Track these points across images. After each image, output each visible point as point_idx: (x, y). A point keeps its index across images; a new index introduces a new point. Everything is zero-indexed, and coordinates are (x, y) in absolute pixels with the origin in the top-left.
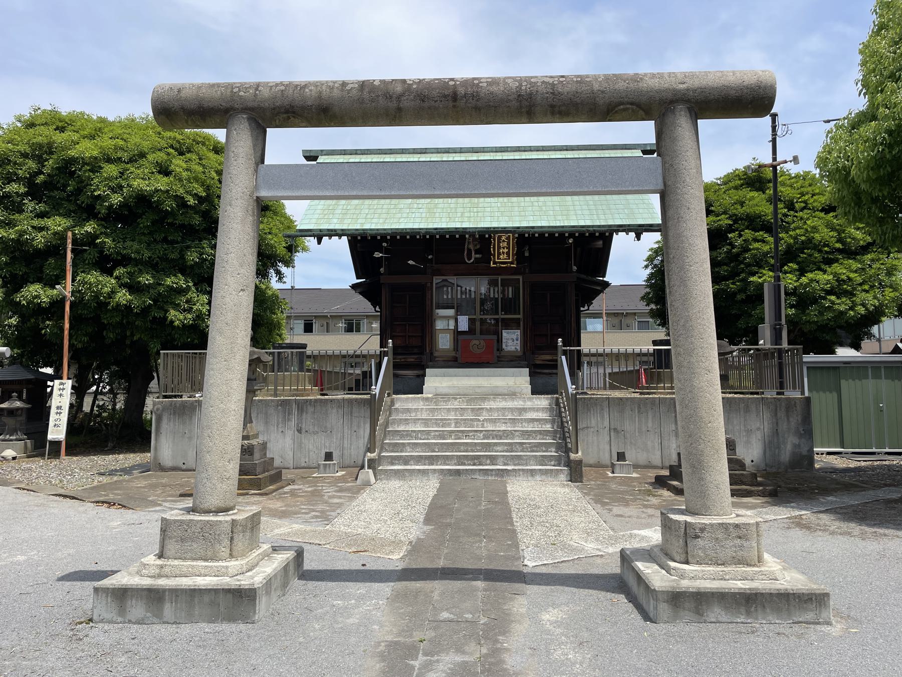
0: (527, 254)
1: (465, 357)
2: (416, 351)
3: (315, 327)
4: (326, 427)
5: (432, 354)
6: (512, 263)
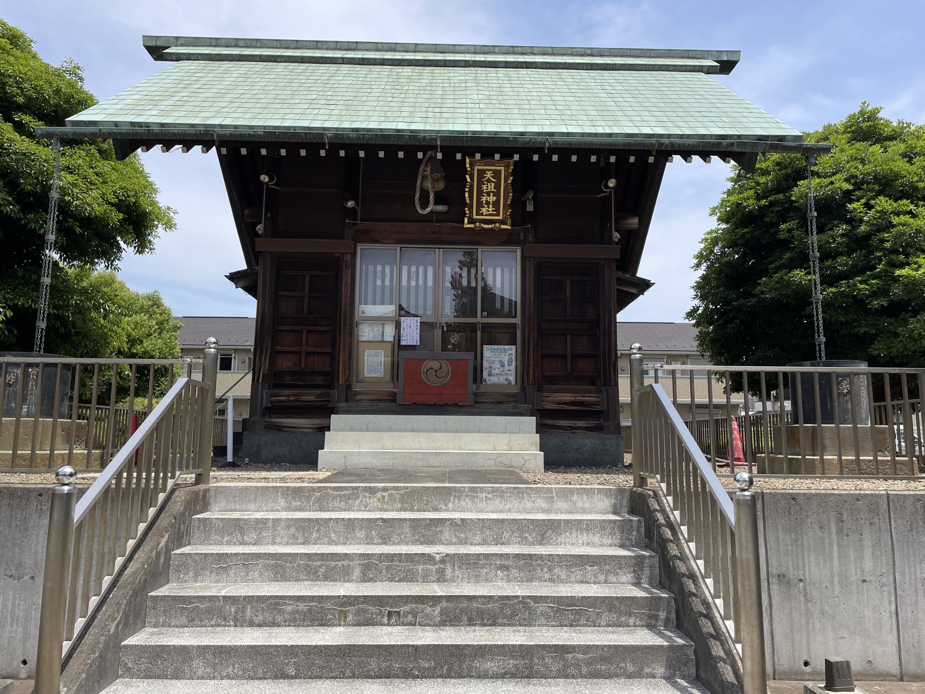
0: (530, 208)
1: (415, 392)
2: (319, 380)
3: (234, 363)
4: (20, 565)
5: (349, 387)
6: (503, 222)
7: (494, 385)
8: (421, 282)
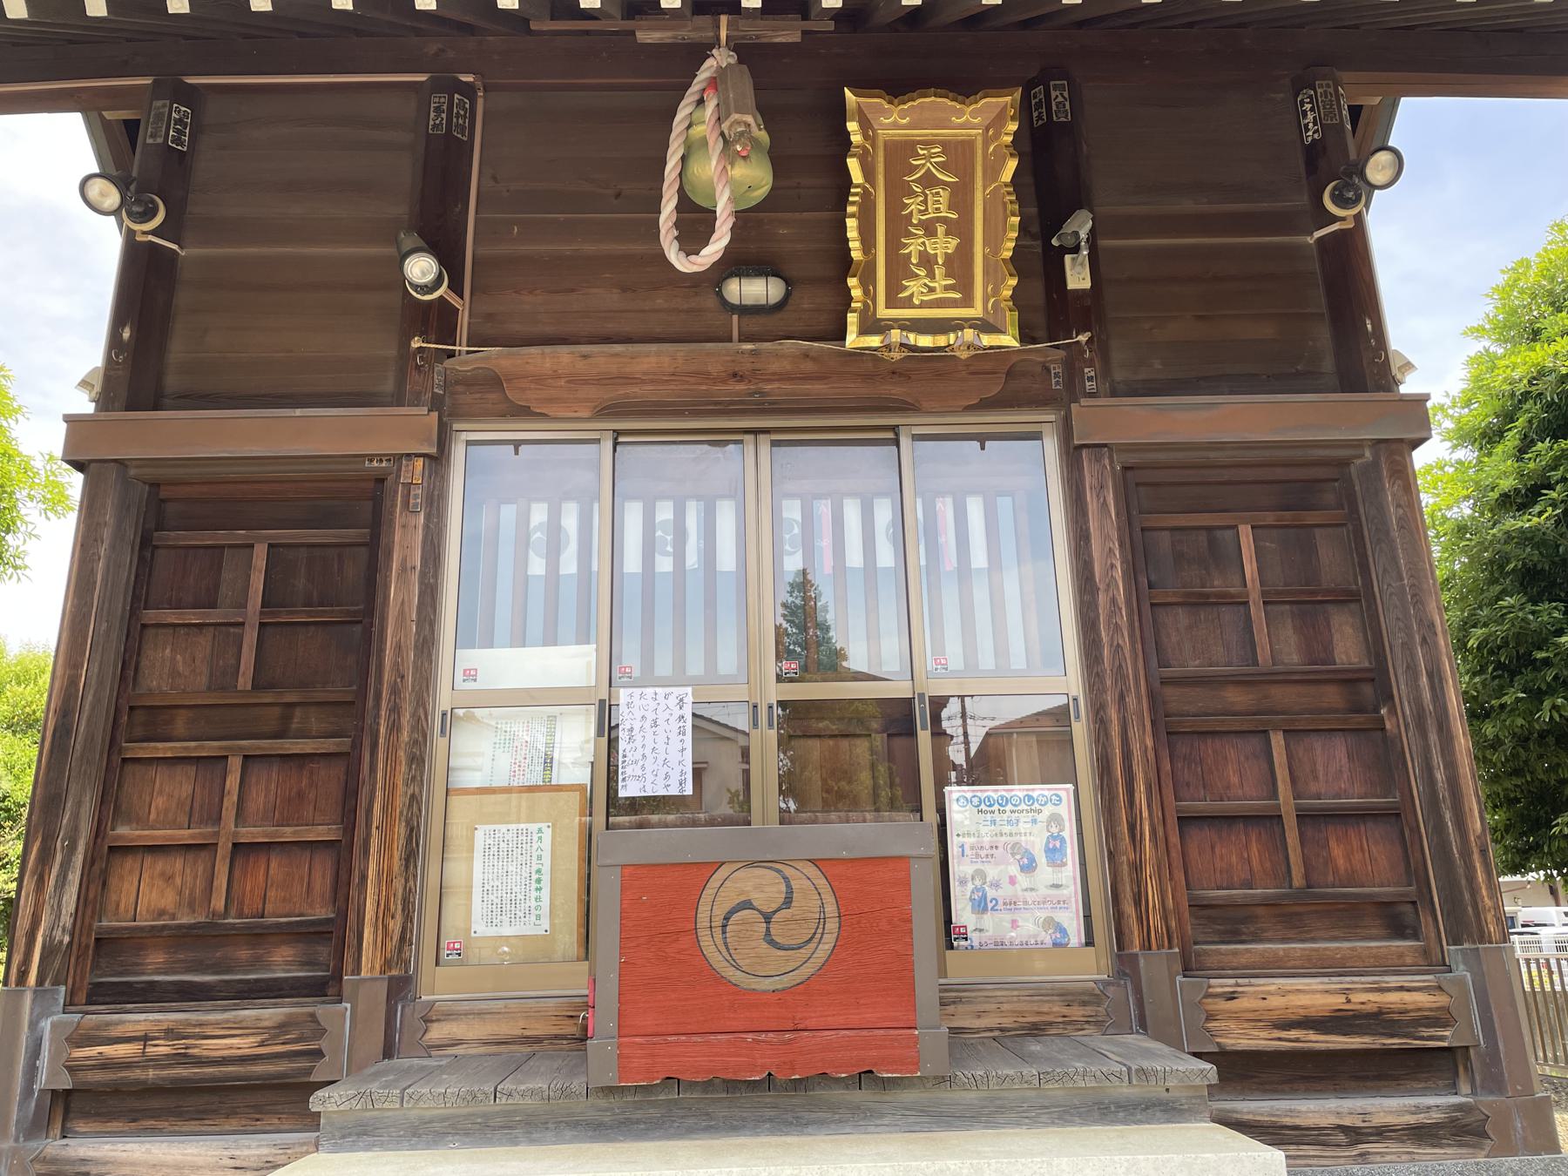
2: (282, 963)
5: (400, 987)
7: (1000, 949)
8: (692, 560)
